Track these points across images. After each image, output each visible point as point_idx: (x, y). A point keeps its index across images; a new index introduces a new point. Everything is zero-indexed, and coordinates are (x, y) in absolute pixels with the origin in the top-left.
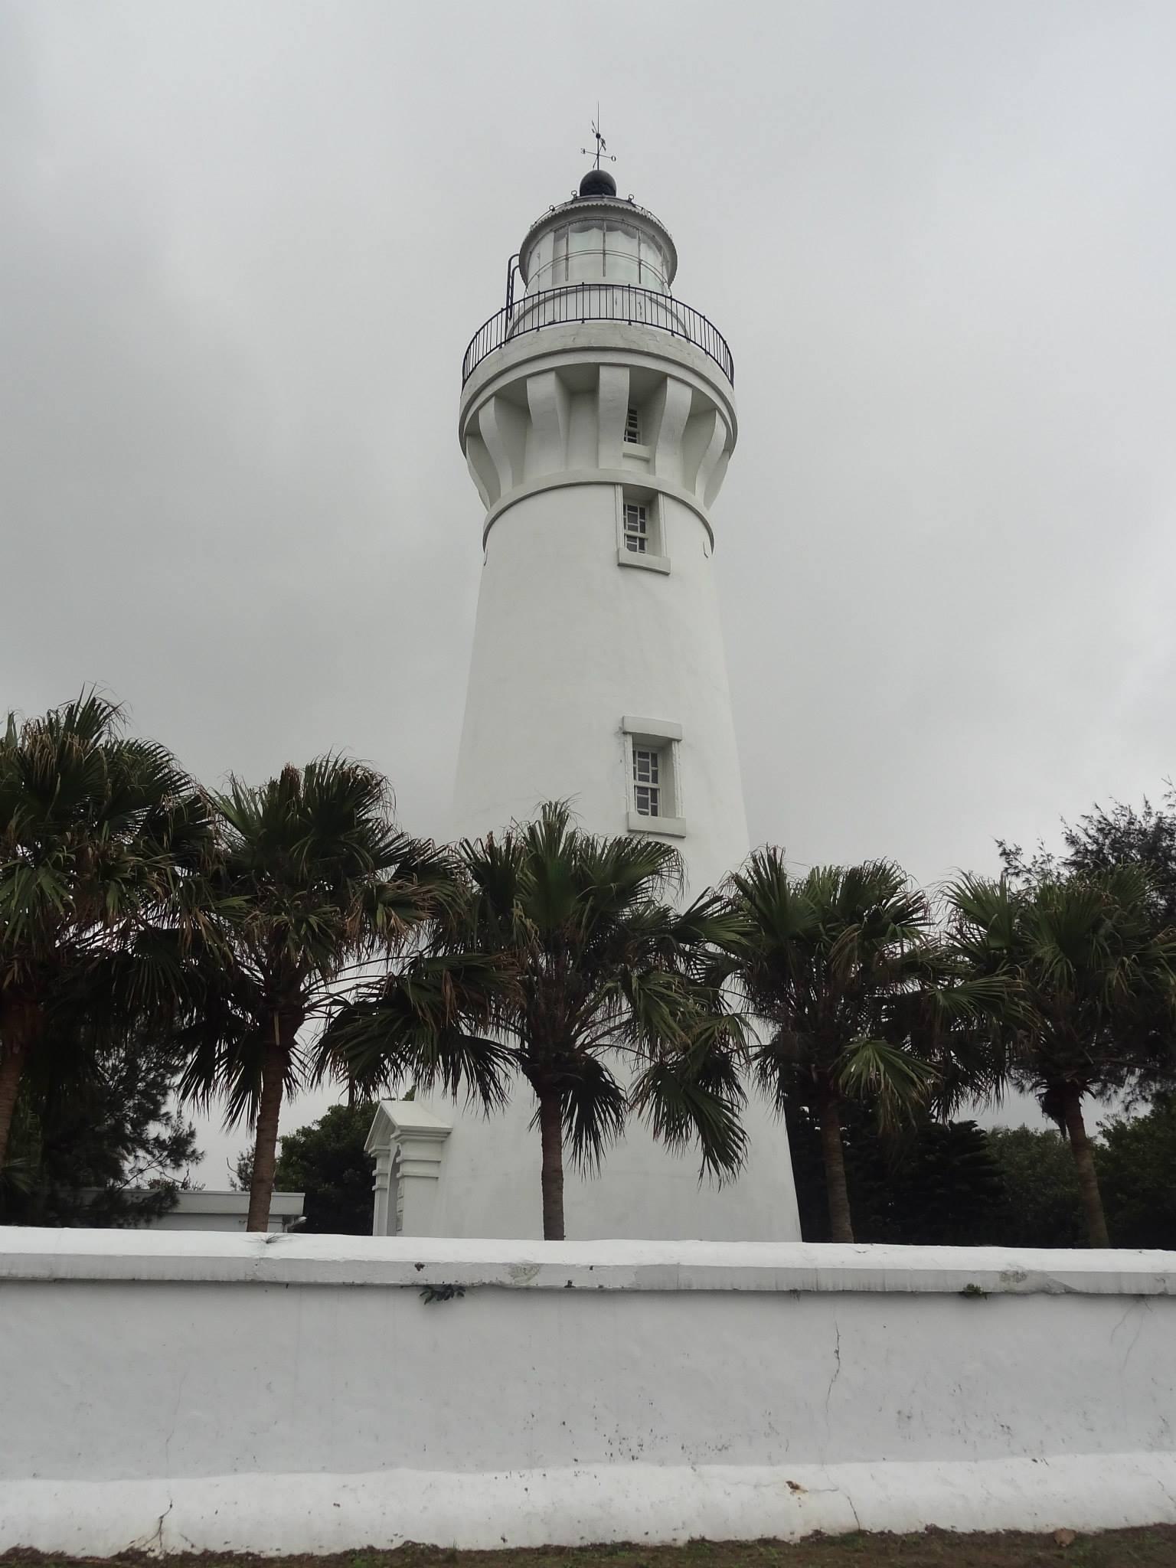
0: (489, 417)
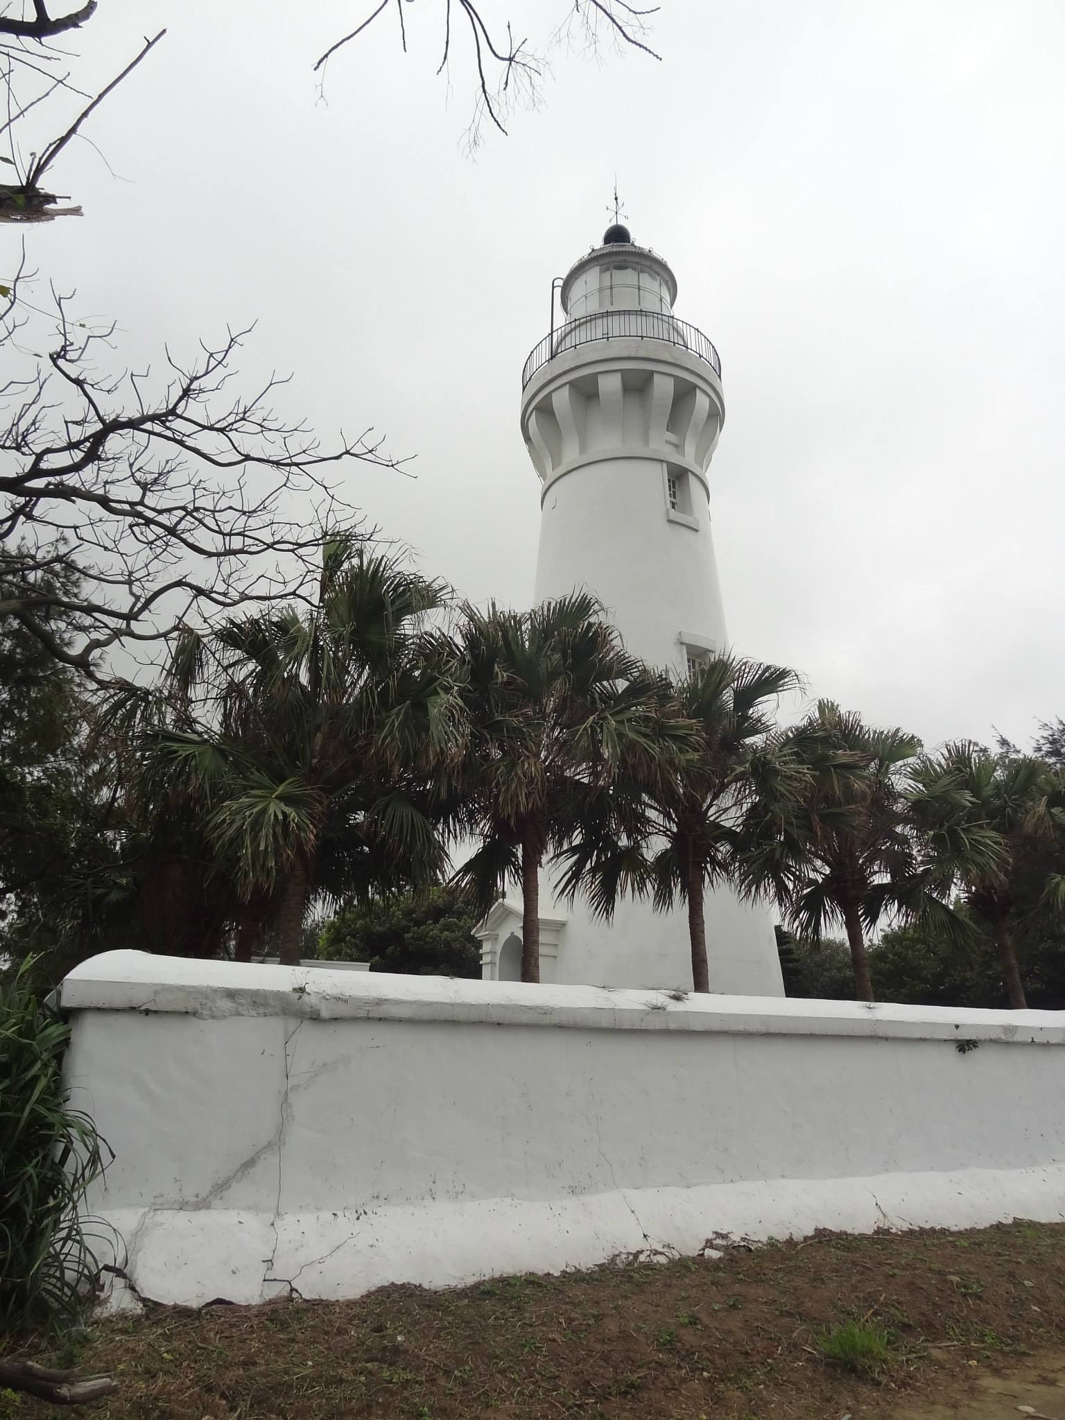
0: (562, 399)
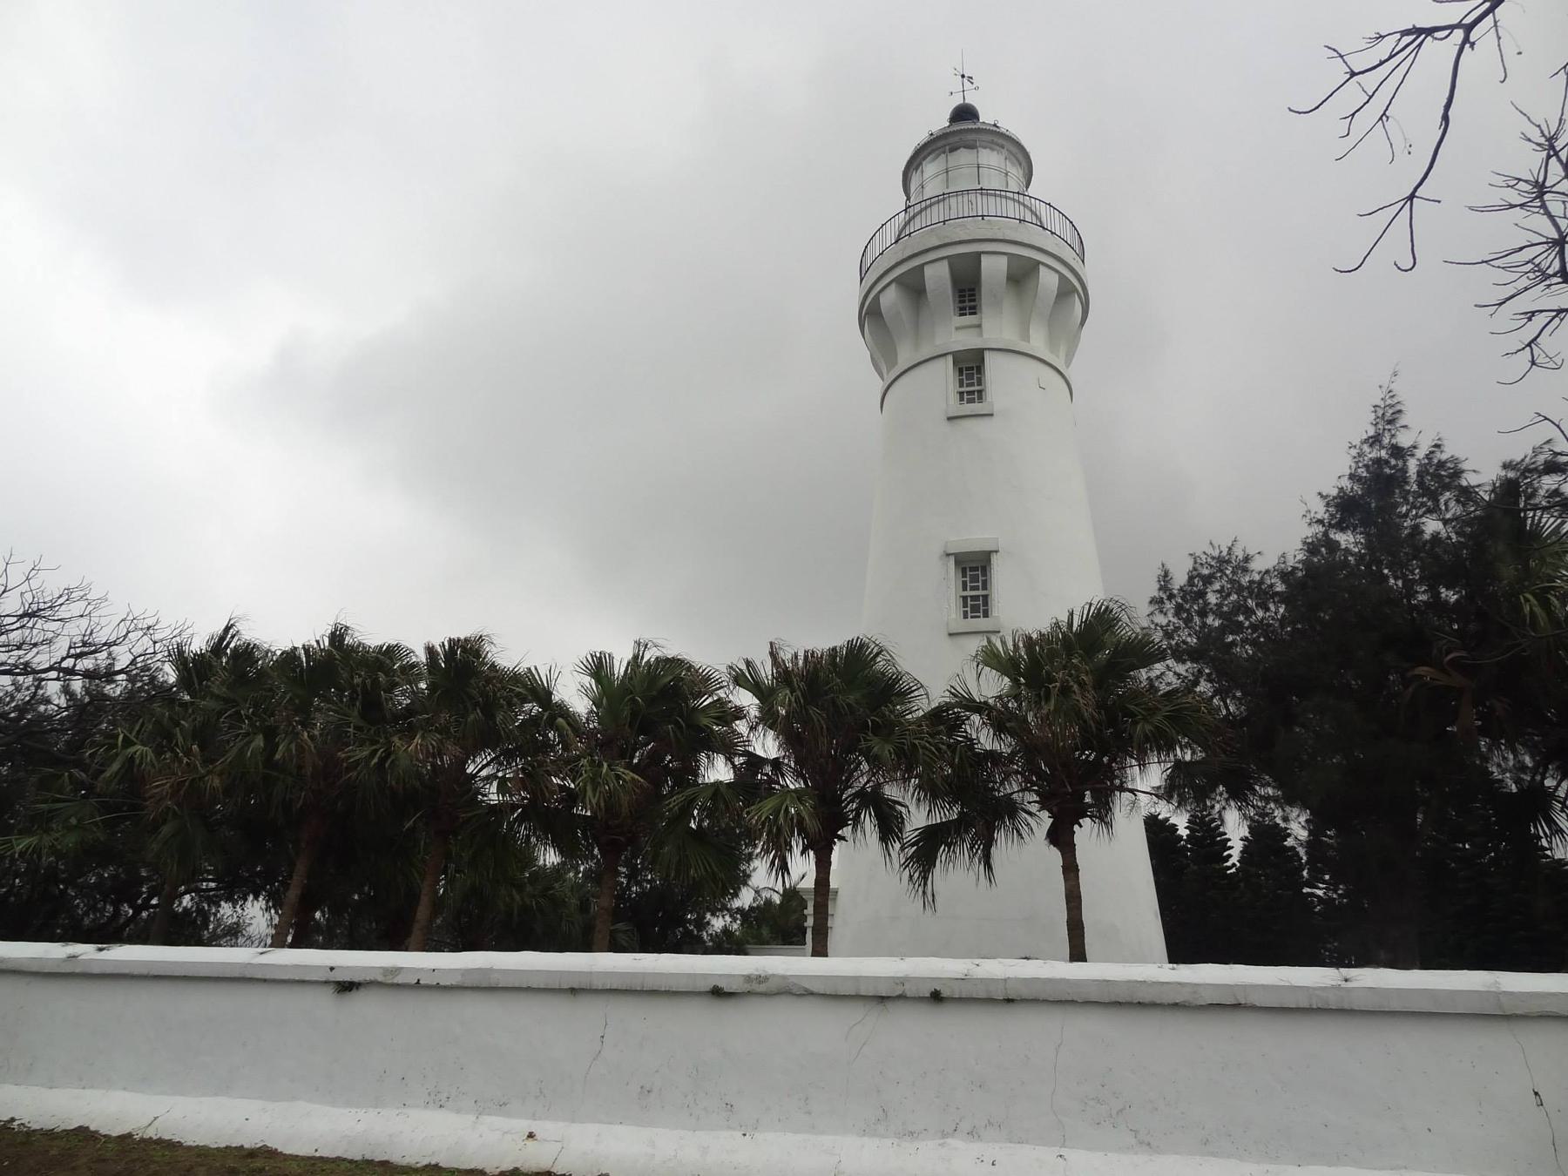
0: (890, 299)
